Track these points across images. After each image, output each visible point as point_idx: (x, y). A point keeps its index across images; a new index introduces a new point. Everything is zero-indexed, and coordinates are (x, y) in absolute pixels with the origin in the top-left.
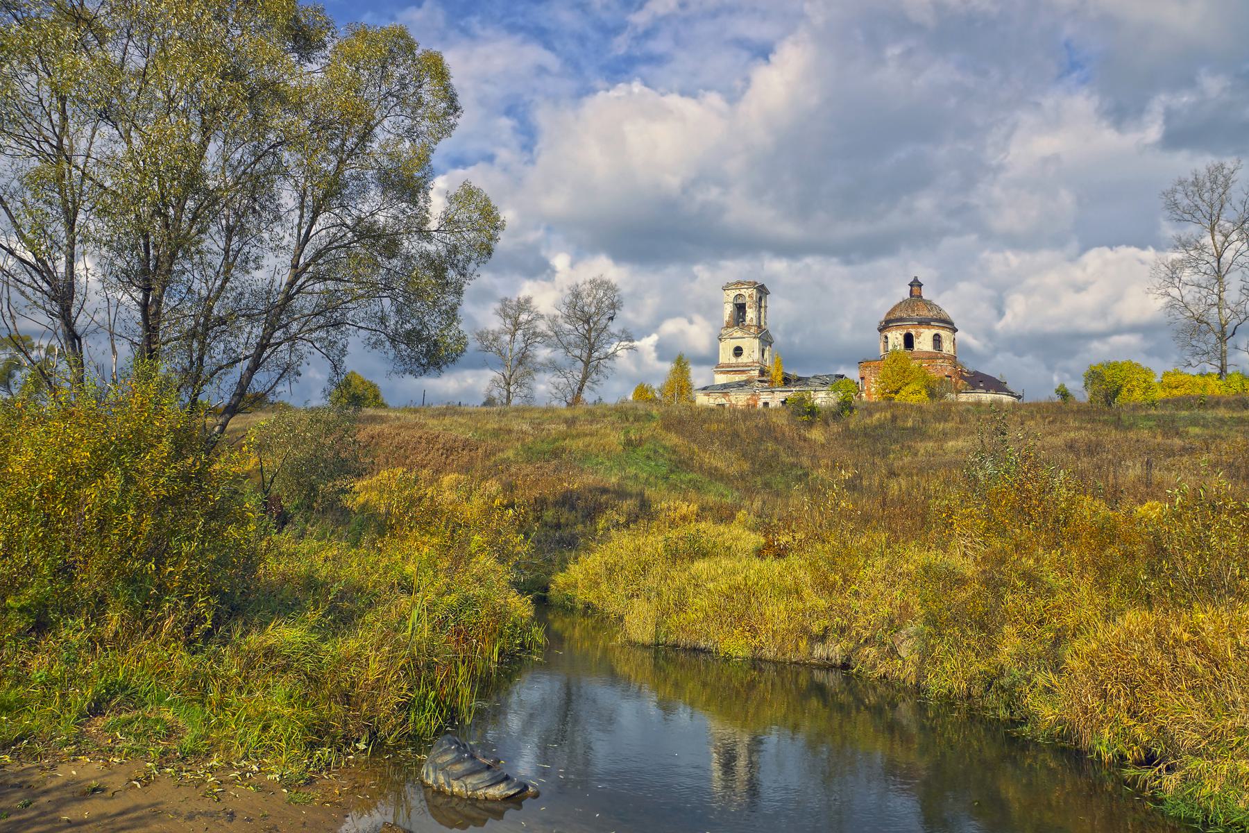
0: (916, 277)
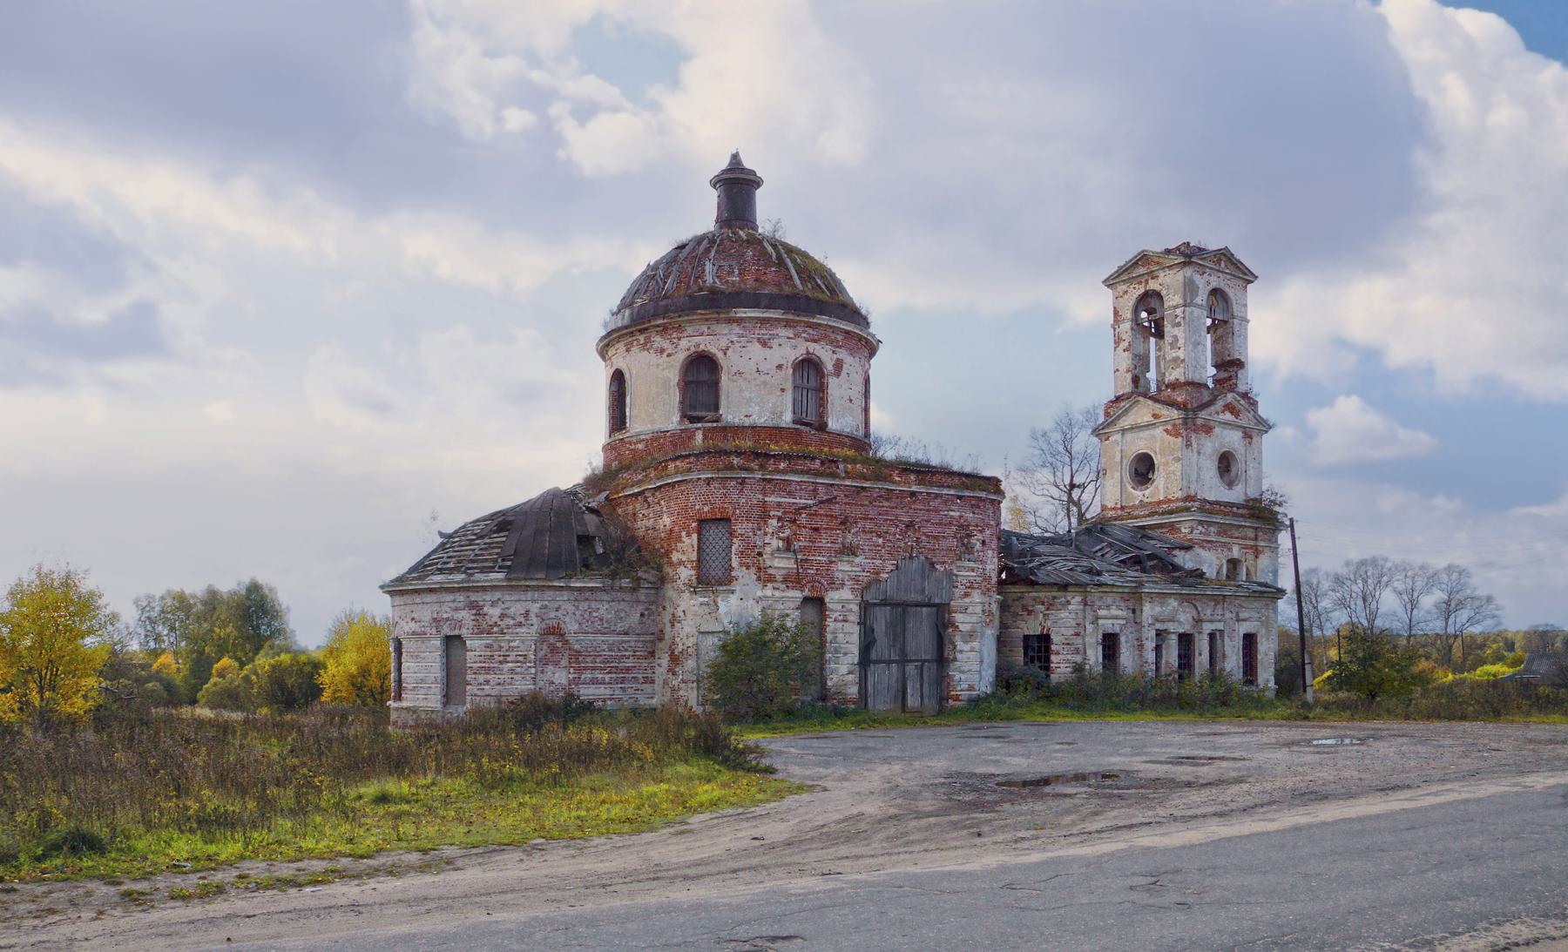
0: (735, 157)
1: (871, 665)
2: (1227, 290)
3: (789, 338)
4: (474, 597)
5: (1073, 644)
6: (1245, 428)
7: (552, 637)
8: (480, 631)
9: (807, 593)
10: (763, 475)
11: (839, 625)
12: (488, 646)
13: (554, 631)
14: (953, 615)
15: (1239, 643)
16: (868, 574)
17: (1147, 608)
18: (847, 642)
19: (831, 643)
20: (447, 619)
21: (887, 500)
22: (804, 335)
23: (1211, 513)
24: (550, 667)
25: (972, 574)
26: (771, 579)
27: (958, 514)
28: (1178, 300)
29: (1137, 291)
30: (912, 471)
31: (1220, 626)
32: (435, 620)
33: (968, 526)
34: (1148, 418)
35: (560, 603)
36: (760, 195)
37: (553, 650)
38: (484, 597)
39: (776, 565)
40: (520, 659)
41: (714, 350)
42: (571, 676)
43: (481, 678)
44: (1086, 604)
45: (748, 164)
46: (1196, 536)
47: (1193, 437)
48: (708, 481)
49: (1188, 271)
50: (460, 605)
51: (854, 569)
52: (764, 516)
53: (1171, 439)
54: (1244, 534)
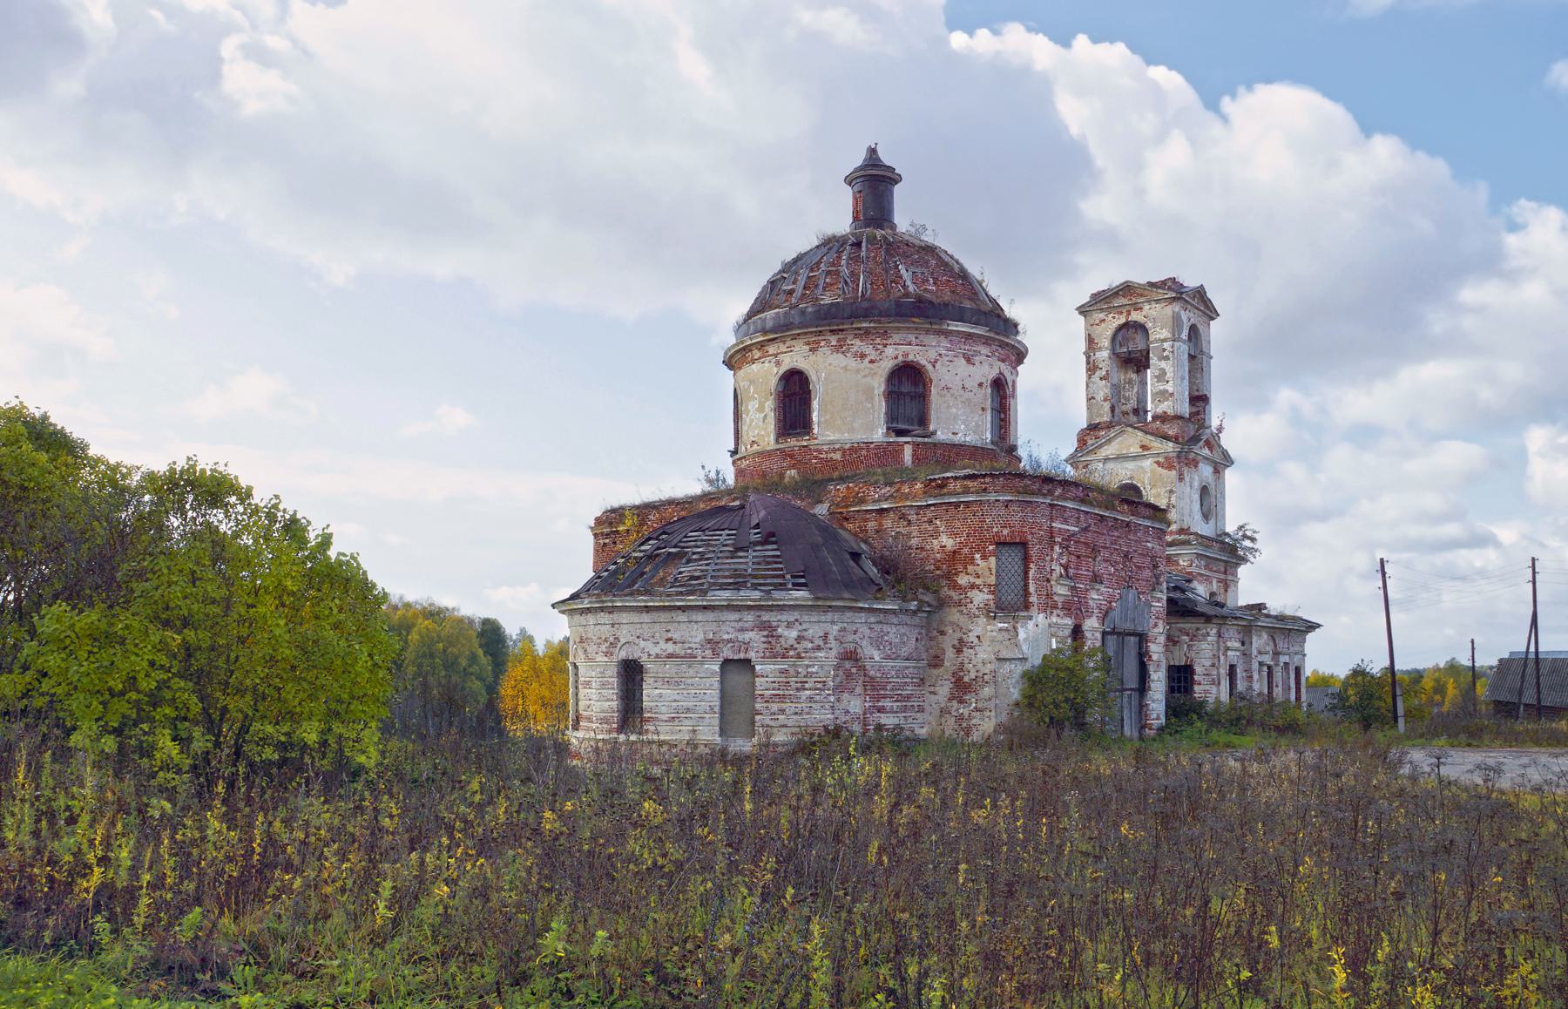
0: (873, 151)
4: (766, 617)
7: (847, 662)
8: (772, 654)
12: (782, 672)
13: (851, 656)
20: (729, 641)
28: (1165, 334)
32: (709, 641)
36: (898, 190)
37: (848, 675)
38: (779, 617)
40: (819, 686)
41: (923, 362)
42: (867, 705)
43: (775, 707)
45: (886, 158)
47: (1186, 472)
48: (1007, 504)
49: (1177, 307)
50: (747, 625)
53: (1164, 472)
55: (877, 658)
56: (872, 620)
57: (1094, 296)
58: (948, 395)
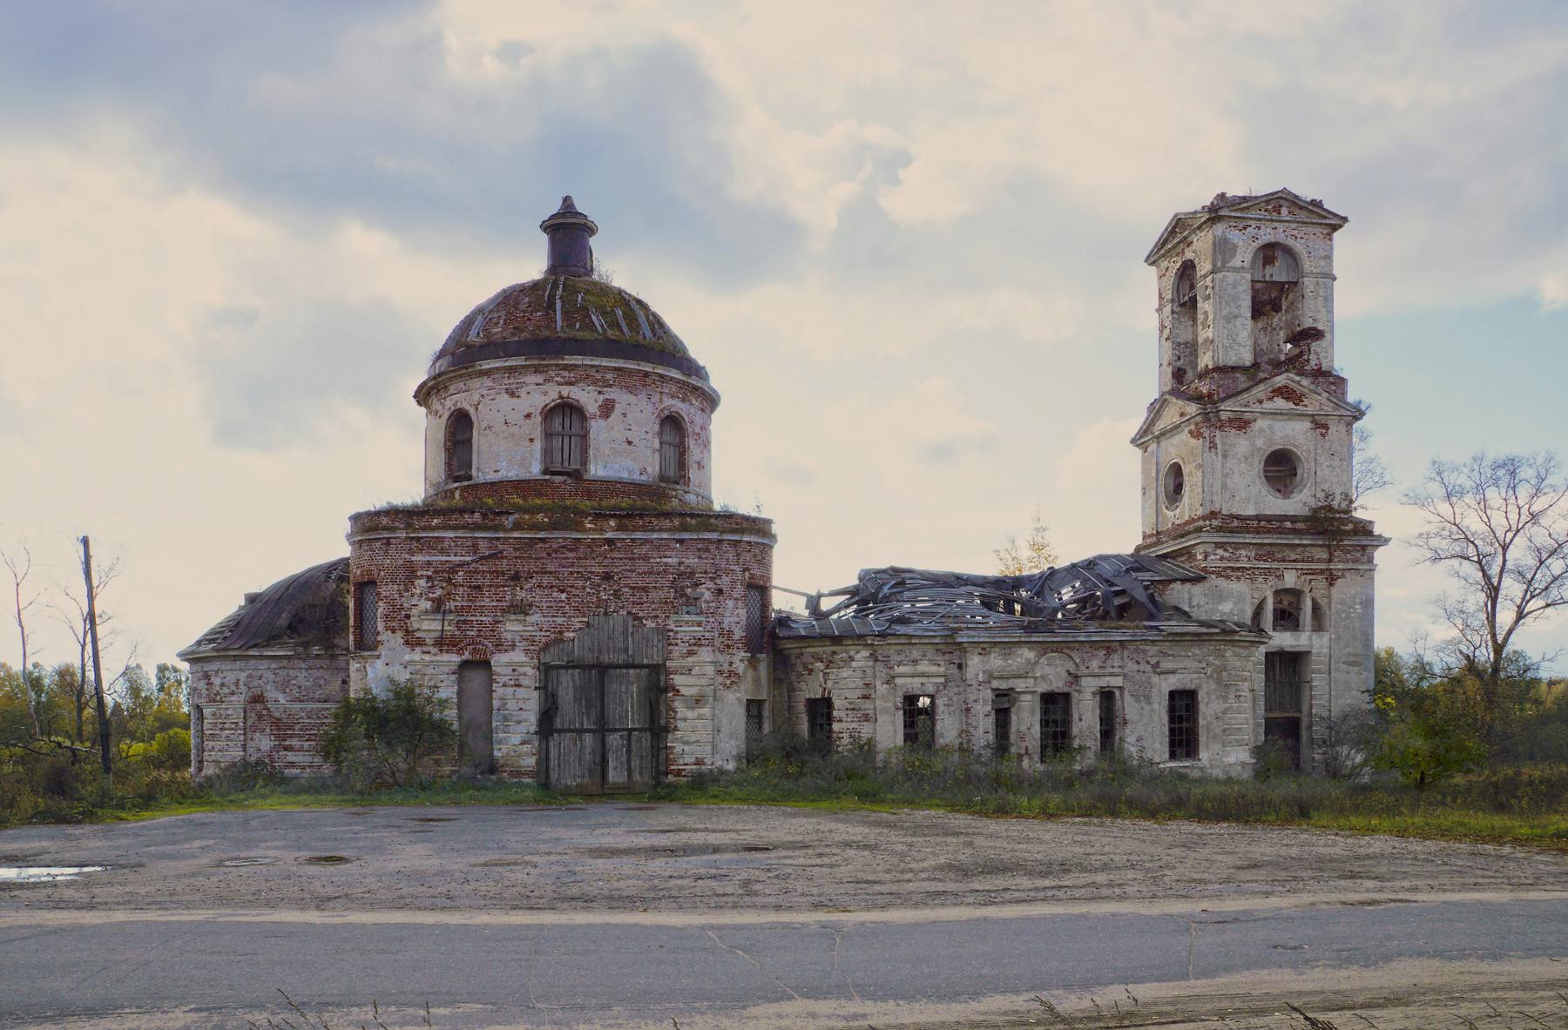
1: (556, 735)
2: (1290, 242)
3: (537, 384)
5: (860, 709)
6: (1313, 415)
9: (467, 656)
10: (407, 533)
11: (510, 690)
13: (258, 699)
14: (672, 676)
15: (1161, 707)
16: (548, 634)
17: (975, 663)
18: (521, 709)
19: (499, 710)
21: (571, 550)
22: (556, 379)
23: (1233, 531)
24: (258, 734)
25: (698, 629)
26: (420, 642)
27: (676, 560)
29: (1175, 265)
30: (611, 516)
31: (1116, 681)
33: (693, 573)
34: (1176, 419)
35: (261, 672)
37: (260, 717)
39: (425, 628)
40: (233, 726)
41: (467, 407)
44: (876, 660)
46: (1214, 561)
51: (527, 628)
52: (411, 573)
54: (1307, 554)
55: (282, 701)
56: (274, 666)
57: (1317, 204)
58: (491, 433)
